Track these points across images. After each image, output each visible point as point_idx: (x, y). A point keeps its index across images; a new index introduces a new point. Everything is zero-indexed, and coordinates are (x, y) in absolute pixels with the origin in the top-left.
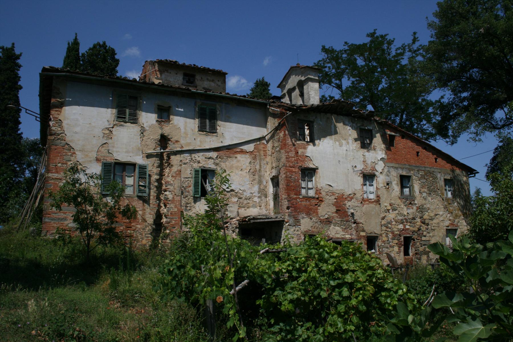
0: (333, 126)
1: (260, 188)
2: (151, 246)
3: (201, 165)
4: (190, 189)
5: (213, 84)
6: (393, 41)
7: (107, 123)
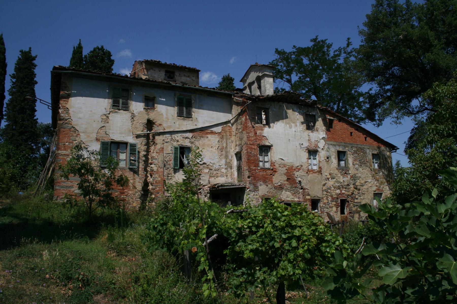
0: (284, 112)
1: (226, 162)
2: (140, 207)
3: (179, 143)
4: (170, 162)
7: (104, 111)
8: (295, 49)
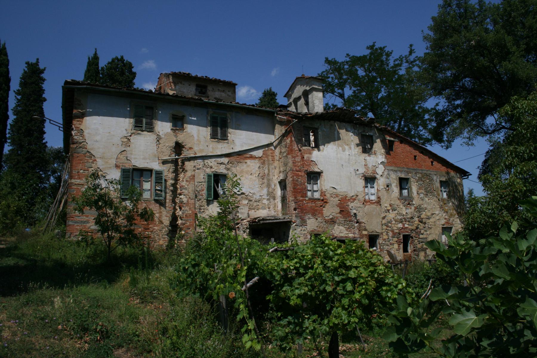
0: (336, 132)
1: (268, 191)
2: (167, 246)
3: (213, 170)
4: (203, 192)
5: (223, 94)
6: (391, 53)
7: (125, 132)
8: (348, 58)
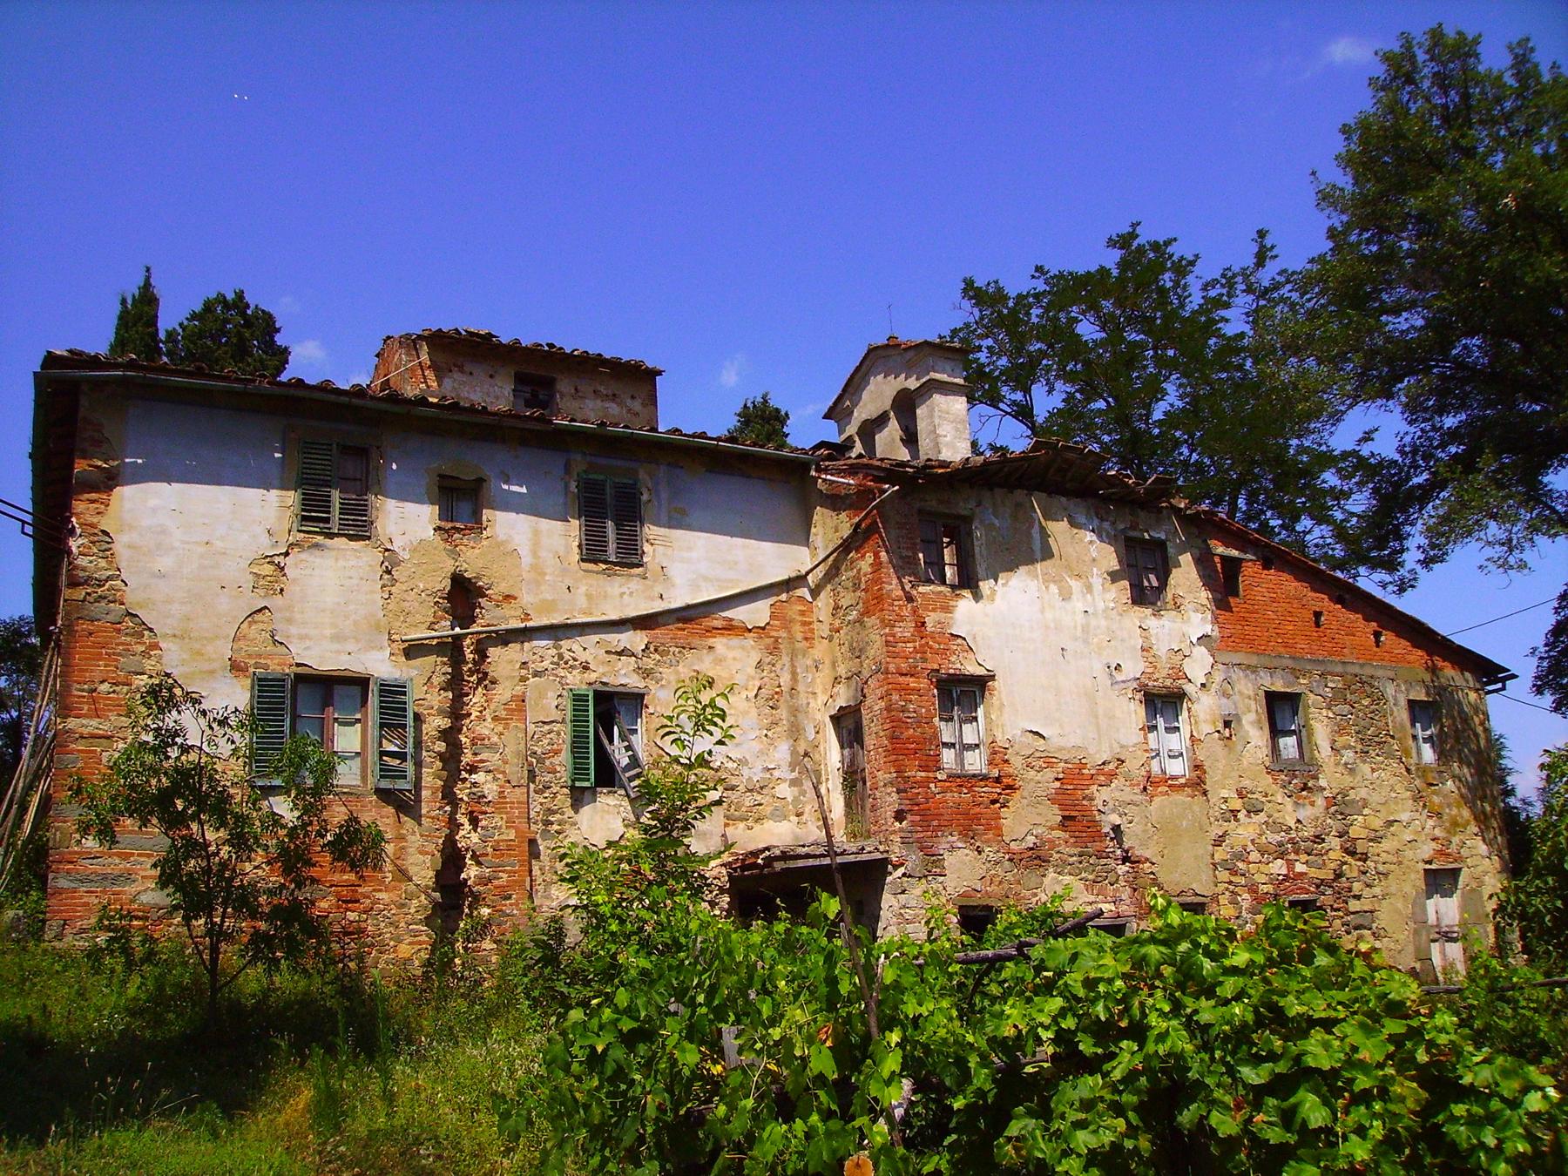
0: (1035, 532)
1: (794, 752)
2: (428, 963)
3: (593, 677)
4: (556, 760)
5: (614, 409)
6: (1192, 263)
7: (265, 540)
8: (1041, 280)
